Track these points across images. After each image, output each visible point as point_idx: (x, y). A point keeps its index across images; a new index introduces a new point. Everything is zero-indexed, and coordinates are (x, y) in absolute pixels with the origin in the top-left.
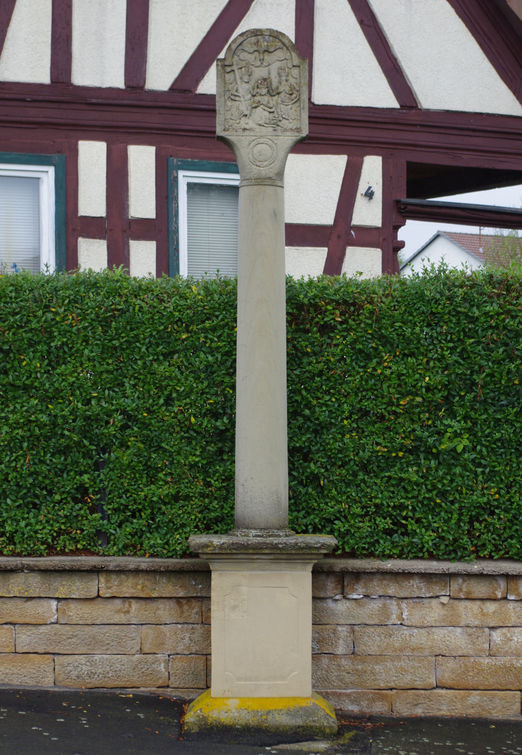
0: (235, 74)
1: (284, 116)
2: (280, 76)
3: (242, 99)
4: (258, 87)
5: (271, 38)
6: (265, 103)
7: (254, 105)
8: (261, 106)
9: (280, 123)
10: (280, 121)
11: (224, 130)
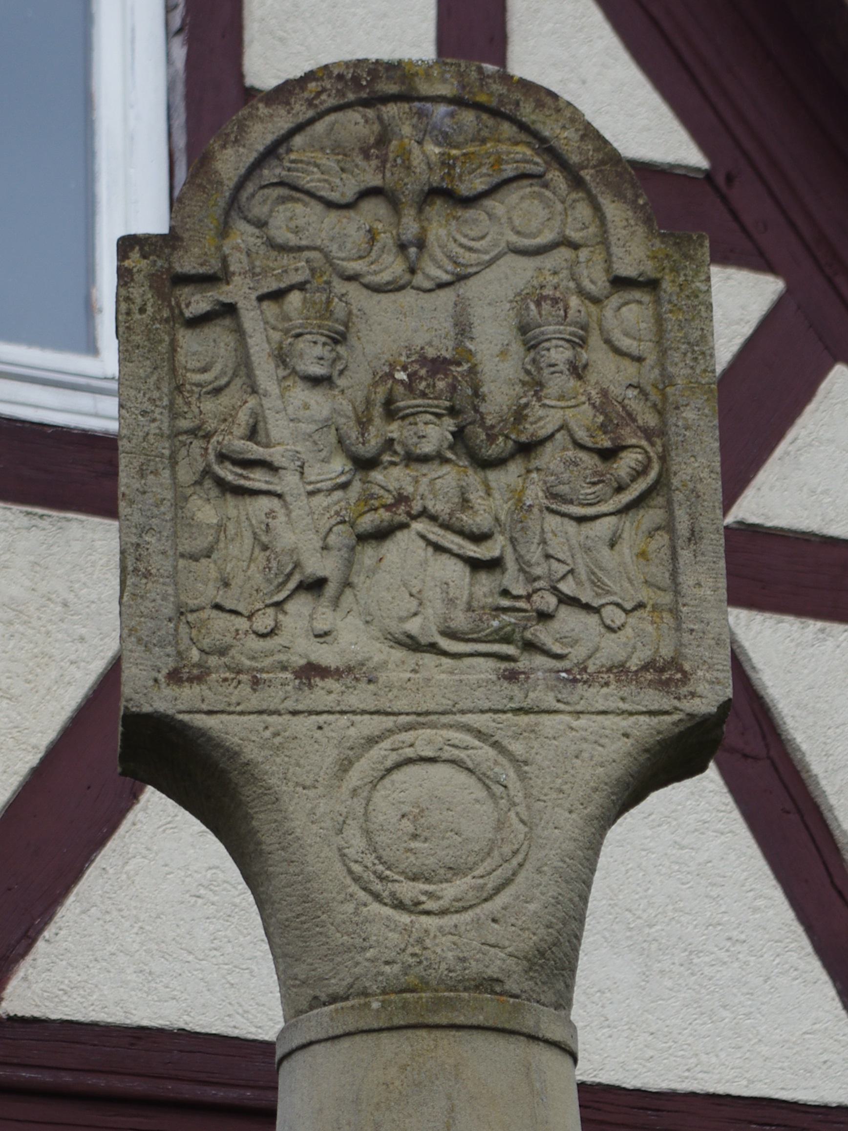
0: (240, 332)
1: (567, 587)
2: (531, 346)
3: (289, 482)
4: (391, 412)
5: (468, 117)
6: (439, 507)
7: (367, 522)
8: (418, 526)
9: (543, 634)
10: (544, 616)
11: (175, 677)
